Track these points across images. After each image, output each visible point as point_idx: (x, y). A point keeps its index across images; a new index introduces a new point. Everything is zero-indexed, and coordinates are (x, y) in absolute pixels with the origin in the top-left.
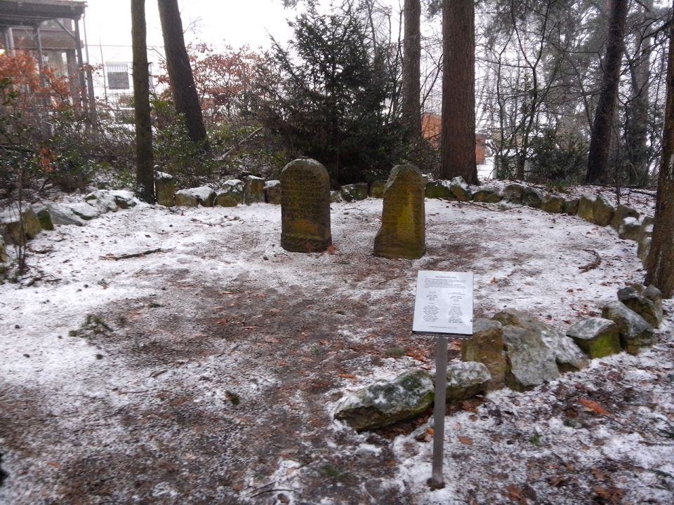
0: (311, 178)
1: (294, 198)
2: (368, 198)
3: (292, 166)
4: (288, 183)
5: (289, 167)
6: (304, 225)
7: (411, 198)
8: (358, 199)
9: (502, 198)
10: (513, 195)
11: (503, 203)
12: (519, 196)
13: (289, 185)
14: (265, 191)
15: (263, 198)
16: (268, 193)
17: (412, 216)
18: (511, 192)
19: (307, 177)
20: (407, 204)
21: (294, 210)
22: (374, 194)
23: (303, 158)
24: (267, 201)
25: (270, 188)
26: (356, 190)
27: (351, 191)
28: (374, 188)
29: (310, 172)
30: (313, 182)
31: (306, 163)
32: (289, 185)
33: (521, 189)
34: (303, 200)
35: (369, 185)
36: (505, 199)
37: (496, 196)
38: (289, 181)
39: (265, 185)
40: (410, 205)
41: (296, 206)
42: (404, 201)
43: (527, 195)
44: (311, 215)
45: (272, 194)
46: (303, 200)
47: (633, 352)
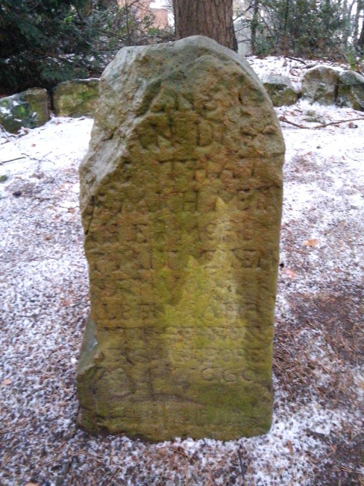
2: (54, 119)
7: (224, 220)
8: (33, 125)
9: (299, 96)
10: (320, 89)
11: (304, 104)
12: (330, 89)
17: (233, 296)
18: (315, 84)
20: (203, 254)
22: (64, 109)
26: (26, 106)
27: (15, 110)
28: (63, 97)
33: (337, 78)
35: (51, 93)
36: (305, 97)
37: (291, 91)
40: (222, 257)
42: (188, 238)
43: (349, 87)
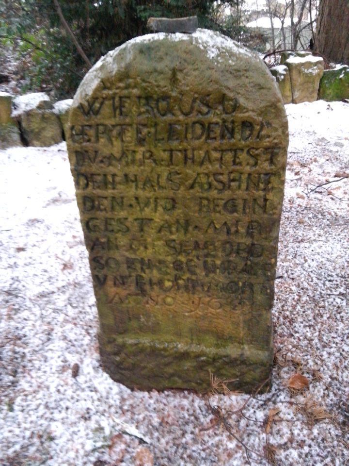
0: (228, 131)
1: (144, 222)
3: (124, 75)
4: (110, 159)
5: (105, 84)
6: (180, 316)
13: (117, 169)
14: (18, 121)
15: (16, 137)
16: (24, 124)
19: (207, 128)
21: (146, 264)
23: (171, 30)
24: (25, 142)
25: (28, 114)
29: (223, 99)
30: (235, 150)
31: (195, 53)
32: (117, 169)
34: (186, 225)
38: (116, 148)
39: (16, 106)
41: (155, 248)
44: (220, 278)
45: (35, 125)
46: (186, 225)
47: (209, 25)
